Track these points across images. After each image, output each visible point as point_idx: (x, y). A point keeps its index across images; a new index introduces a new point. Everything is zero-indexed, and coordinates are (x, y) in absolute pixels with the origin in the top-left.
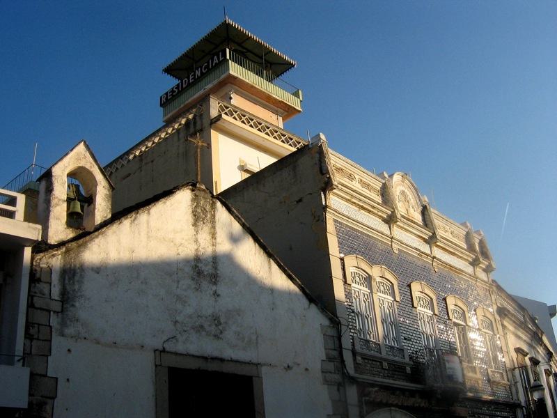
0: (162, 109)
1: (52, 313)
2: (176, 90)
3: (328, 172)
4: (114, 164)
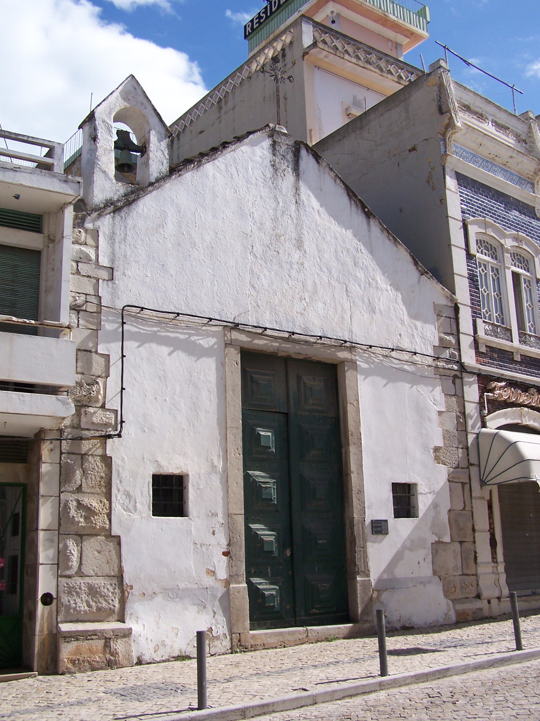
0: (246, 42)
1: (100, 281)
2: (264, 15)
3: (449, 111)
4: (188, 115)
